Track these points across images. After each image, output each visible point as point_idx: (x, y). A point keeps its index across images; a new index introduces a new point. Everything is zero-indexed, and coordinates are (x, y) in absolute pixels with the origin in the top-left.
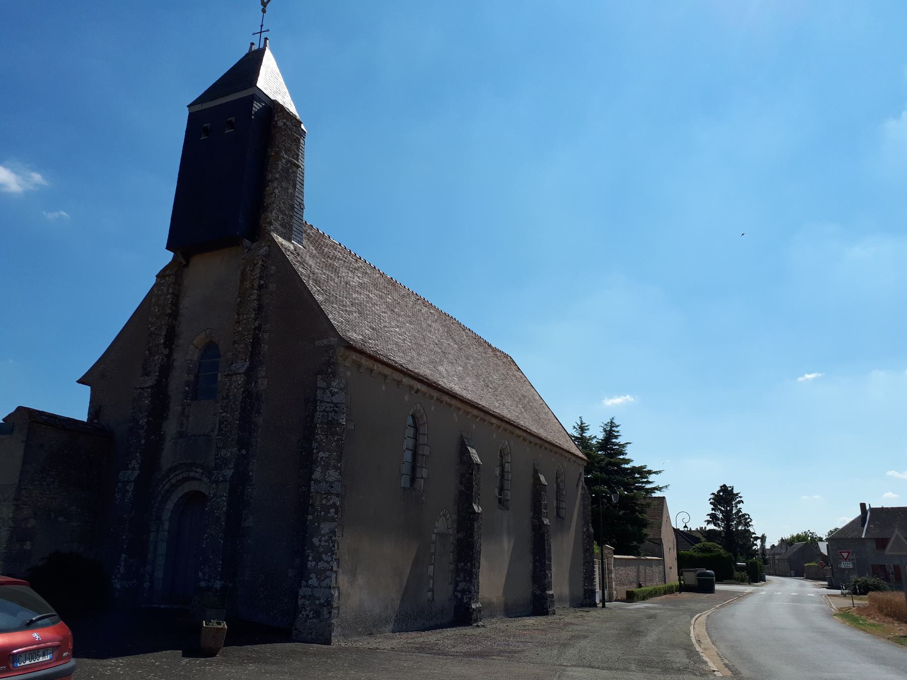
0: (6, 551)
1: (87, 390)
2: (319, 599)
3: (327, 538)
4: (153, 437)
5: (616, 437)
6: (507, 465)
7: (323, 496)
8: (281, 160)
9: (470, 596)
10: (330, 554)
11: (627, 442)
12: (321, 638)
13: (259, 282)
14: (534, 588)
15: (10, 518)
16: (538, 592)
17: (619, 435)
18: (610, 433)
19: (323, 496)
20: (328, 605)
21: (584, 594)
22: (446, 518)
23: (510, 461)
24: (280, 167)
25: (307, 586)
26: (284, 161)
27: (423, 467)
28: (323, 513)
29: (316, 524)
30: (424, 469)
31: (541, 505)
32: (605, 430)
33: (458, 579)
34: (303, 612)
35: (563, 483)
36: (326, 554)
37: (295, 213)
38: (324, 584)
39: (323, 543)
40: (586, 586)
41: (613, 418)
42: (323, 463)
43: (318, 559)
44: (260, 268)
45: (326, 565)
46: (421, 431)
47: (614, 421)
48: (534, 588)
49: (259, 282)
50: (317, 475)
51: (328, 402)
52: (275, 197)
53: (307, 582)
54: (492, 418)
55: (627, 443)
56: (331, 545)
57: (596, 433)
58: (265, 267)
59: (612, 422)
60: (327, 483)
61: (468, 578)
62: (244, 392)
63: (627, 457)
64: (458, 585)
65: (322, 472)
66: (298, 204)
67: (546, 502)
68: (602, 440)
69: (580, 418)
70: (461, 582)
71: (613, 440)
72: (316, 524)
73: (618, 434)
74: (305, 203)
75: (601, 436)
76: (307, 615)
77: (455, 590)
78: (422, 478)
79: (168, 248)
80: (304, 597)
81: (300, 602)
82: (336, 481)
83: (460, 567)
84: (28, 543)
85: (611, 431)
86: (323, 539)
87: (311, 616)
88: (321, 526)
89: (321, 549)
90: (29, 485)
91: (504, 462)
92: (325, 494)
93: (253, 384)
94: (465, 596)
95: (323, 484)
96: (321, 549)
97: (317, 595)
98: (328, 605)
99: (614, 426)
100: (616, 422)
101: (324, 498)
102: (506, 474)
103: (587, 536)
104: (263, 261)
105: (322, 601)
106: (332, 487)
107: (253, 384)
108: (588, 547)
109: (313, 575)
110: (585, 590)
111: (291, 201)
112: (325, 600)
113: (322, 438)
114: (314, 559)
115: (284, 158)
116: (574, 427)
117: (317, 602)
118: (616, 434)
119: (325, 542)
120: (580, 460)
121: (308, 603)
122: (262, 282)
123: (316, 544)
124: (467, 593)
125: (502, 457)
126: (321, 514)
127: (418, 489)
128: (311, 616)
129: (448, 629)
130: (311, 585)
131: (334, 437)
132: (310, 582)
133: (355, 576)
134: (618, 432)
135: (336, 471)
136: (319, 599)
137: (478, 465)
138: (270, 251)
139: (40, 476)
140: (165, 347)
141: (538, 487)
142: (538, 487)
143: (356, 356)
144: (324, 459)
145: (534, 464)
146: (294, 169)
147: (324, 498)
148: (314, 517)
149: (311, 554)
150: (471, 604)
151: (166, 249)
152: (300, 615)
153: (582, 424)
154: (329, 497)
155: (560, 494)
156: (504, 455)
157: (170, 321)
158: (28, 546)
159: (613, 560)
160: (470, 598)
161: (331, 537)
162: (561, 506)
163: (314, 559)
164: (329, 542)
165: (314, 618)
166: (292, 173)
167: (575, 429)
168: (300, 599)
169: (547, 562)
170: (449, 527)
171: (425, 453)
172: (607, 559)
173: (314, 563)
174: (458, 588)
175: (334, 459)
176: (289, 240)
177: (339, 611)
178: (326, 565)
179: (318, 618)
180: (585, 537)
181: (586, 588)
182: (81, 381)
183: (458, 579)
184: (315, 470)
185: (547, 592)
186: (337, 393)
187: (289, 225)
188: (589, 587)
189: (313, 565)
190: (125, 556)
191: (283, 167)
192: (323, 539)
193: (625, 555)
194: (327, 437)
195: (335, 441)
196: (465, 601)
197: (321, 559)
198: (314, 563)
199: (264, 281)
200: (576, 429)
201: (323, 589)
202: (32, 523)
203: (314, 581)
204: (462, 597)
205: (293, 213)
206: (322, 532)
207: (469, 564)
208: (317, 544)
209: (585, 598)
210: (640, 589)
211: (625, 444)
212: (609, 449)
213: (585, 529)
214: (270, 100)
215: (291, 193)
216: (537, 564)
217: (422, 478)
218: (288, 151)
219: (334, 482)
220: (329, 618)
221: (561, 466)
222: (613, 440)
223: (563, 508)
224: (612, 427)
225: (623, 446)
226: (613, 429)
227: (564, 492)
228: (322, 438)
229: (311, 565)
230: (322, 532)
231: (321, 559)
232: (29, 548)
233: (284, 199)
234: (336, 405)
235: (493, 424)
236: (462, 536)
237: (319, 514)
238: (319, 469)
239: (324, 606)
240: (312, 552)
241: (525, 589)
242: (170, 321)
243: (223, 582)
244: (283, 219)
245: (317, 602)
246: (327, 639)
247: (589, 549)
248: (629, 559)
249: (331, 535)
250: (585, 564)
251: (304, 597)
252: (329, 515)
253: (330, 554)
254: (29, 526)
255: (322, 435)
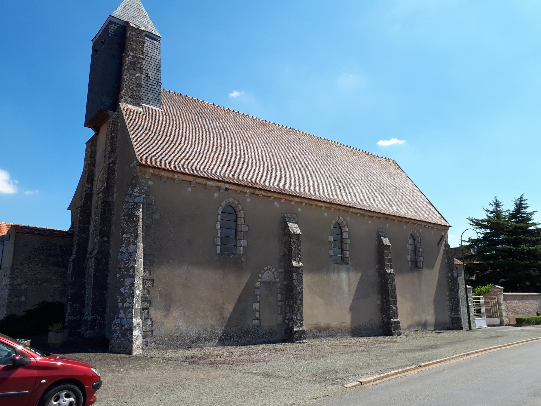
0: (8, 302)
1: (70, 211)
2: (124, 326)
3: (129, 288)
4: (83, 235)
5: (525, 208)
6: (344, 234)
7: (126, 262)
8: (128, 57)
9: (293, 322)
10: (131, 298)
11: (535, 211)
12: (126, 350)
13: (111, 135)
14: (383, 317)
15: (9, 285)
16: (386, 320)
17: (528, 206)
18: (520, 206)
19: (126, 262)
20: (130, 330)
21: (452, 321)
22: (272, 272)
23: (347, 231)
24: (128, 62)
25: (118, 318)
26: (131, 57)
27: (241, 239)
28: (126, 273)
29: (122, 280)
30: (242, 240)
31: (384, 259)
32: (516, 205)
33: (286, 311)
34: (115, 334)
35: (420, 243)
36: (129, 298)
37: (142, 88)
38: (128, 316)
39: (127, 291)
40: (452, 315)
41: (523, 195)
42: (126, 242)
43: (124, 301)
44: (112, 126)
45: (129, 305)
46: (239, 216)
47: (524, 197)
48: (383, 317)
49: (111, 135)
50: (123, 249)
51: (131, 203)
52: (125, 81)
53: (118, 315)
54: (318, 202)
55: (534, 212)
56: (132, 292)
57: (508, 207)
58: (115, 125)
59: (521, 198)
60: (128, 253)
61: (291, 311)
62: (103, 203)
63: (534, 221)
64: (286, 316)
65: (126, 247)
66: (156, 83)
67: (390, 257)
68: (513, 211)
69: (495, 197)
70: (288, 313)
71: (522, 211)
72: (122, 280)
73: (527, 206)
74: (162, 81)
75: (512, 208)
76: (118, 336)
77: (285, 319)
78: (241, 246)
79: (86, 125)
80: (116, 325)
81: (113, 328)
82: (134, 252)
83: (287, 303)
84: (23, 297)
85: (520, 204)
86: (127, 288)
87: (120, 336)
88: (125, 281)
89: (126, 295)
90: (20, 266)
91: (342, 232)
92: (126, 260)
93: (110, 198)
94: (290, 323)
95: (126, 255)
96: (126, 295)
97: (123, 323)
98: (130, 330)
99: (523, 200)
100: (525, 197)
101: (126, 263)
102: (344, 240)
103: (451, 280)
104: (113, 121)
105: (126, 327)
106: (131, 256)
107: (110, 198)
108: (453, 287)
109: (121, 311)
110: (452, 318)
111: (139, 81)
112: (128, 326)
113: (125, 225)
114: (122, 301)
115: (131, 56)
116: (490, 204)
117: (123, 328)
118: (525, 206)
119: (128, 290)
120: (440, 226)
121: (118, 328)
122: (113, 134)
123: (122, 292)
124: (291, 320)
125: (341, 229)
126: (124, 273)
127: (239, 254)
128: (120, 336)
129: (260, 345)
130: (120, 317)
131: (132, 224)
132: (120, 315)
133: (169, 311)
134: (526, 204)
135: (134, 245)
136: (124, 326)
137: (298, 235)
138: (118, 115)
139: (28, 261)
140: (88, 183)
141: (381, 247)
142: (381, 247)
143: (153, 171)
144: (127, 238)
145: (378, 231)
146: (140, 61)
147: (126, 263)
148: (120, 275)
149: (119, 298)
150: (293, 328)
151: (84, 126)
152: (114, 336)
153: (497, 201)
154: (129, 262)
155: (417, 252)
156: (342, 227)
157: (89, 168)
158: (23, 299)
159: (502, 296)
160: (293, 324)
161: (131, 287)
162: (419, 260)
163: (122, 301)
164: (130, 291)
165: (121, 337)
166: (138, 64)
167: (491, 206)
168: (113, 326)
169: (391, 299)
170: (276, 277)
171: (242, 230)
172: (497, 295)
173: (121, 304)
174: (287, 318)
175: (133, 238)
176: (139, 105)
177: (152, 334)
178: (129, 305)
179: (125, 338)
180: (450, 281)
181: (452, 316)
182: (68, 209)
183: (286, 311)
184: (121, 246)
185: (392, 320)
186: (139, 196)
187: (138, 96)
188: (456, 316)
189: (121, 305)
190: (70, 303)
191: (130, 61)
192: (127, 288)
193: (529, 292)
194: (128, 225)
195: (133, 227)
196: (290, 326)
197: (126, 301)
198: (121, 304)
199: (115, 134)
200: (492, 205)
201: (127, 320)
202: (24, 286)
203: (122, 315)
204: (289, 323)
205: (141, 88)
206: (126, 284)
207: (291, 301)
208: (123, 292)
209: (453, 324)
210: (538, 317)
211: (532, 212)
212: (518, 217)
213: (450, 275)
214: (123, 22)
215: (139, 76)
216: (384, 300)
217: (241, 246)
218: (134, 50)
219: (133, 253)
220: (131, 338)
221: (416, 232)
222: (522, 211)
223: (421, 261)
224: (521, 201)
225: (530, 214)
226: (522, 202)
227: (421, 250)
228: (125, 225)
229: (120, 305)
230: (126, 284)
231: (126, 301)
232: (24, 300)
233: (132, 81)
234: (136, 204)
235: (322, 206)
236: (287, 283)
237: (123, 273)
238: (124, 245)
239: (128, 330)
240: (120, 297)
241: (446, 318)
242: (89, 168)
243: (94, 316)
244: (133, 94)
245: (123, 328)
246: (130, 351)
247: (453, 289)
248: (525, 295)
249: (131, 286)
250: (450, 299)
251: (116, 325)
252: (130, 273)
253: (131, 298)
254: (22, 288)
255: (125, 223)
